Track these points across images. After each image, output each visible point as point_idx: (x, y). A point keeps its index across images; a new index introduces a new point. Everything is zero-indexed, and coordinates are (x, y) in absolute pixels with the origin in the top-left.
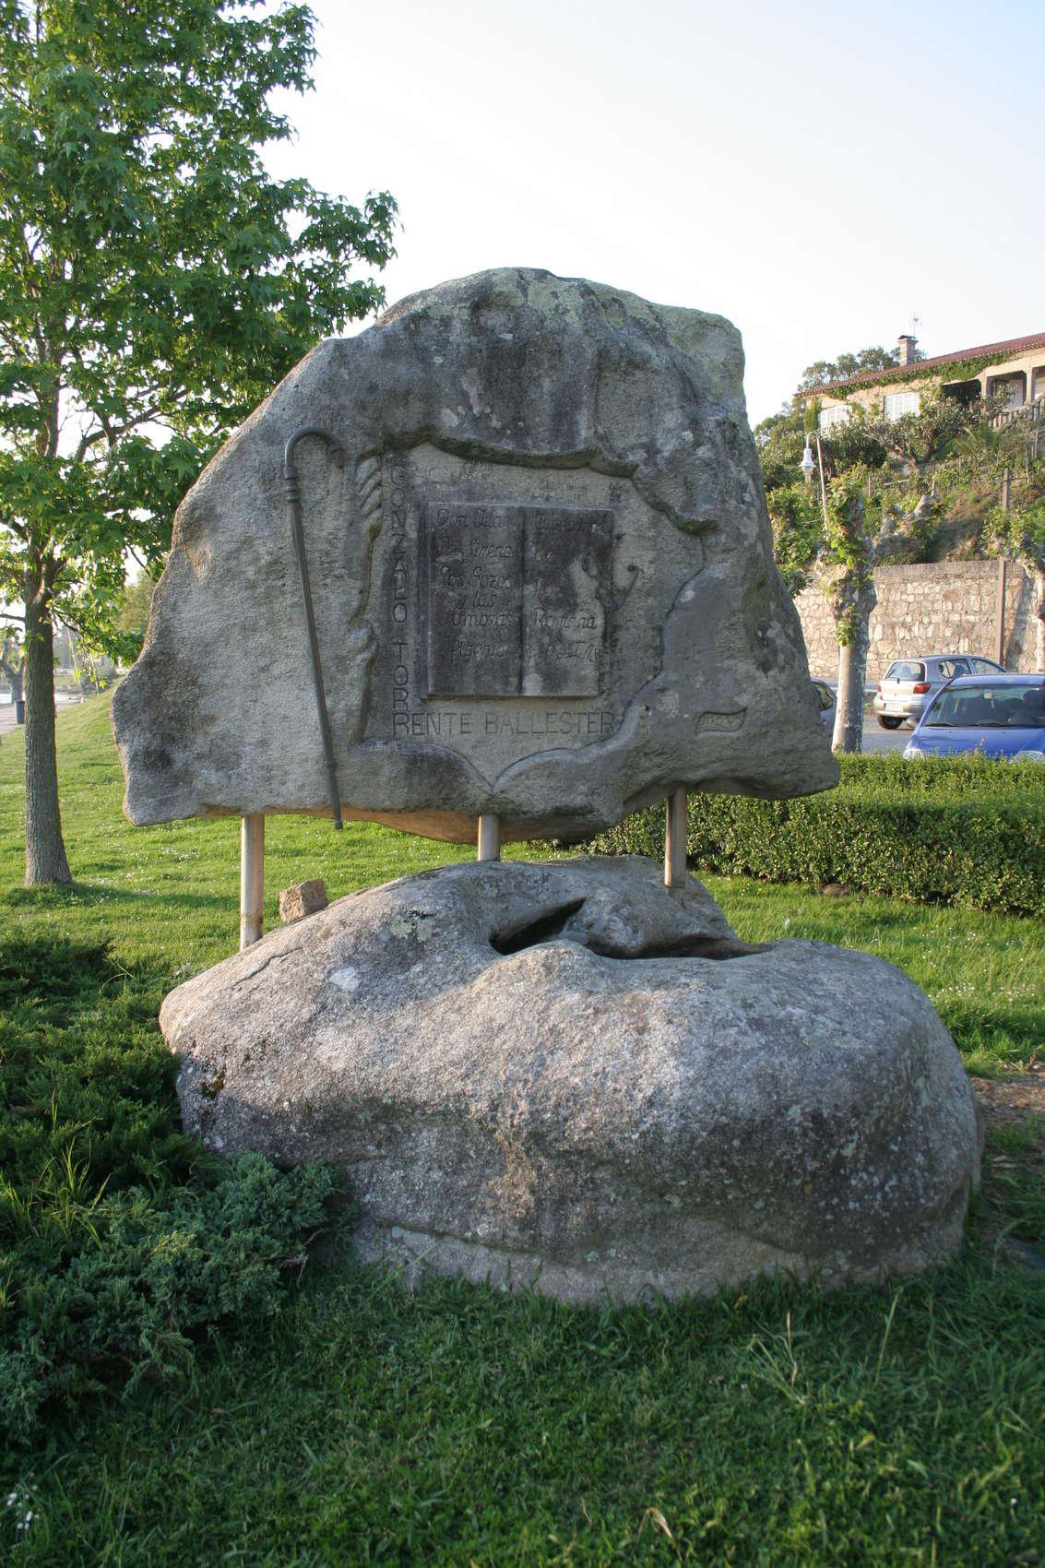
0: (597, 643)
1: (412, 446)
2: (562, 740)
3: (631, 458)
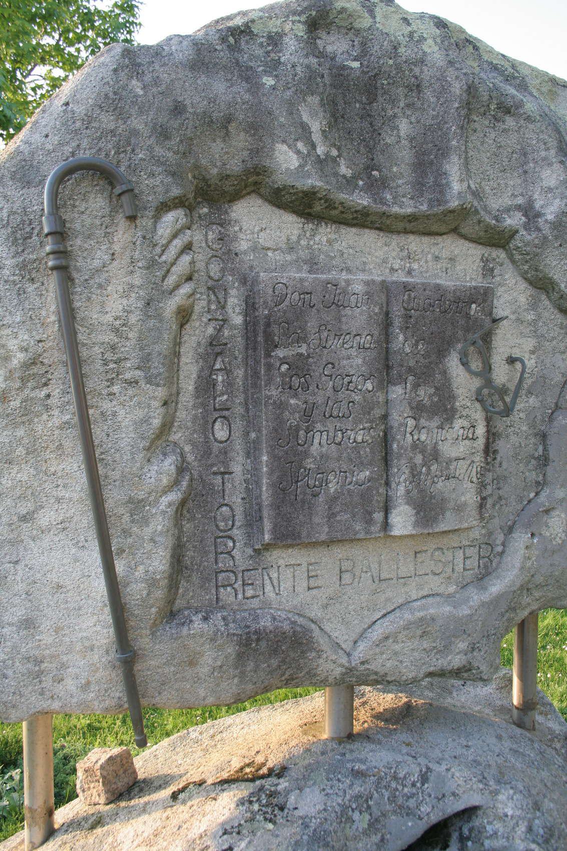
0: (479, 458)
1: (235, 197)
2: (434, 584)
3: (509, 222)
